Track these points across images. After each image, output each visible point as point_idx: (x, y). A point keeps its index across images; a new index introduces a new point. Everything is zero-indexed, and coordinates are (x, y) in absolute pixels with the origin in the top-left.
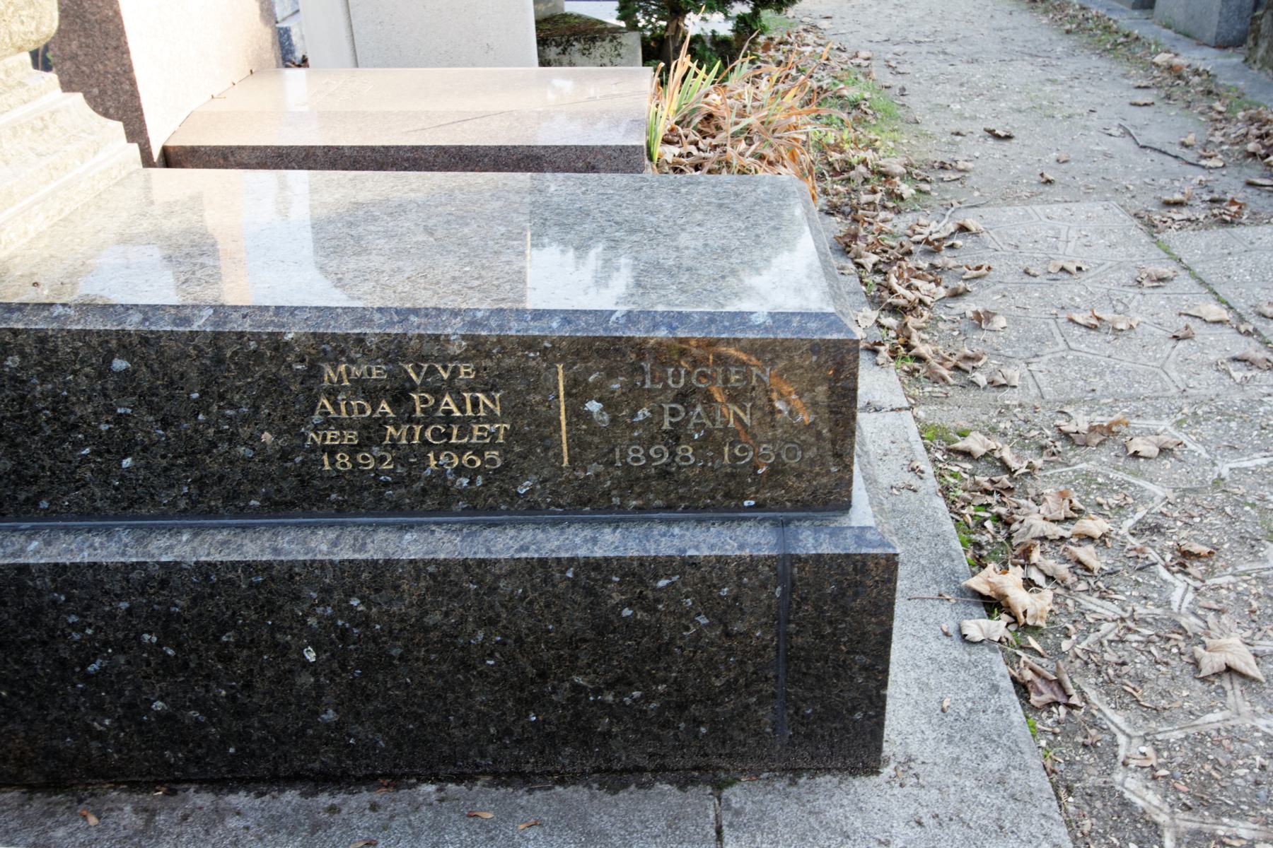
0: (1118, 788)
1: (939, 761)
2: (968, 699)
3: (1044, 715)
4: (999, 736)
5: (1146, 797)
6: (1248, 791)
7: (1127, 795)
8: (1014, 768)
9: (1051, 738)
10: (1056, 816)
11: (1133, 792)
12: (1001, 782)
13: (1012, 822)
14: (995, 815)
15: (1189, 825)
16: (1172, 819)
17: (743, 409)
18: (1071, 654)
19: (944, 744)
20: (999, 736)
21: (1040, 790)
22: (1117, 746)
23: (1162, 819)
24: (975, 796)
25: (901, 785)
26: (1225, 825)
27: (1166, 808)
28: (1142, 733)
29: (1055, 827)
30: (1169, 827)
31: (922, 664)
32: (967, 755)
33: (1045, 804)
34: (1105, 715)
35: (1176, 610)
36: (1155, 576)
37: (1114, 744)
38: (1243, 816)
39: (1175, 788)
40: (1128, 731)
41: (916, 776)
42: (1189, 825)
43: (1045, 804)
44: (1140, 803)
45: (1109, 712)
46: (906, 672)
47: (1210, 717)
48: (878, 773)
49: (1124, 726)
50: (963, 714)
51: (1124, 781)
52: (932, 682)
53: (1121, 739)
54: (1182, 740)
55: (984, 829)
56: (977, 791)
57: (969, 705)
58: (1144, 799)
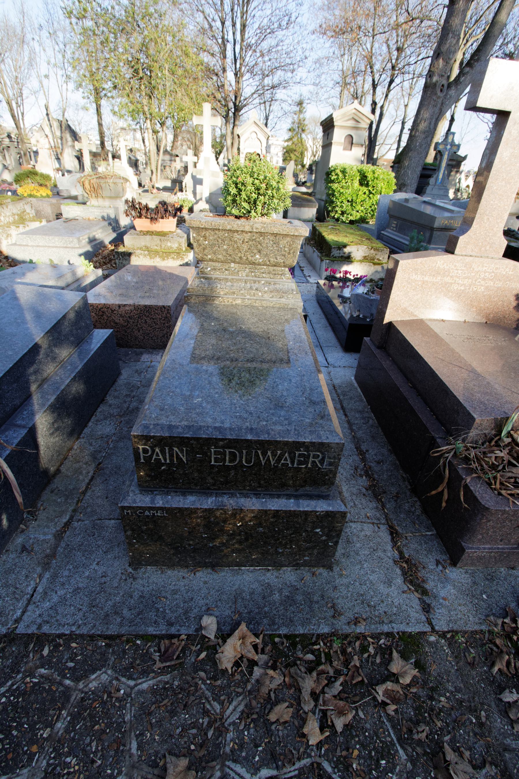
0: (104, 669)
1: (132, 590)
2: (165, 610)
3: (156, 648)
4: (141, 619)
5: (96, 681)
6: (81, 742)
7: (99, 672)
8: (122, 620)
9: (142, 648)
10: (93, 631)
11: (99, 676)
12: (116, 613)
13: (95, 611)
14: (100, 605)
15: (74, 697)
16: (80, 690)
17: (182, 451)
18: (195, 676)
19: (140, 594)
20: (141, 619)
21: (108, 628)
22: (128, 679)
23: (81, 685)
24: (111, 600)
25: (122, 573)
26: (67, 717)
27: (86, 690)
28: (133, 696)
29: (88, 629)
30: (76, 686)
31: (189, 594)
32: (132, 602)
33: (100, 628)
34: (150, 680)
35: (227, 763)
36: (263, 764)
37: (130, 678)
38: (67, 731)
39: (96, 701)
40: (136, 688)
41: (126, 580)
42: (74, 697)
43: (100, 628)
44: (93, 677)
45: (151, 682)
46: (185, 586)
47: (134, 745)
48: (129, 566)
49: (139, 687)
50: (156, 605)
51: (108, 674)
52: (178, 596)
53: (131, 683)
54: (124, 719)
55: (95, 600)
56: (113, 601)
57: (161, 609)
58: (94, 680)
